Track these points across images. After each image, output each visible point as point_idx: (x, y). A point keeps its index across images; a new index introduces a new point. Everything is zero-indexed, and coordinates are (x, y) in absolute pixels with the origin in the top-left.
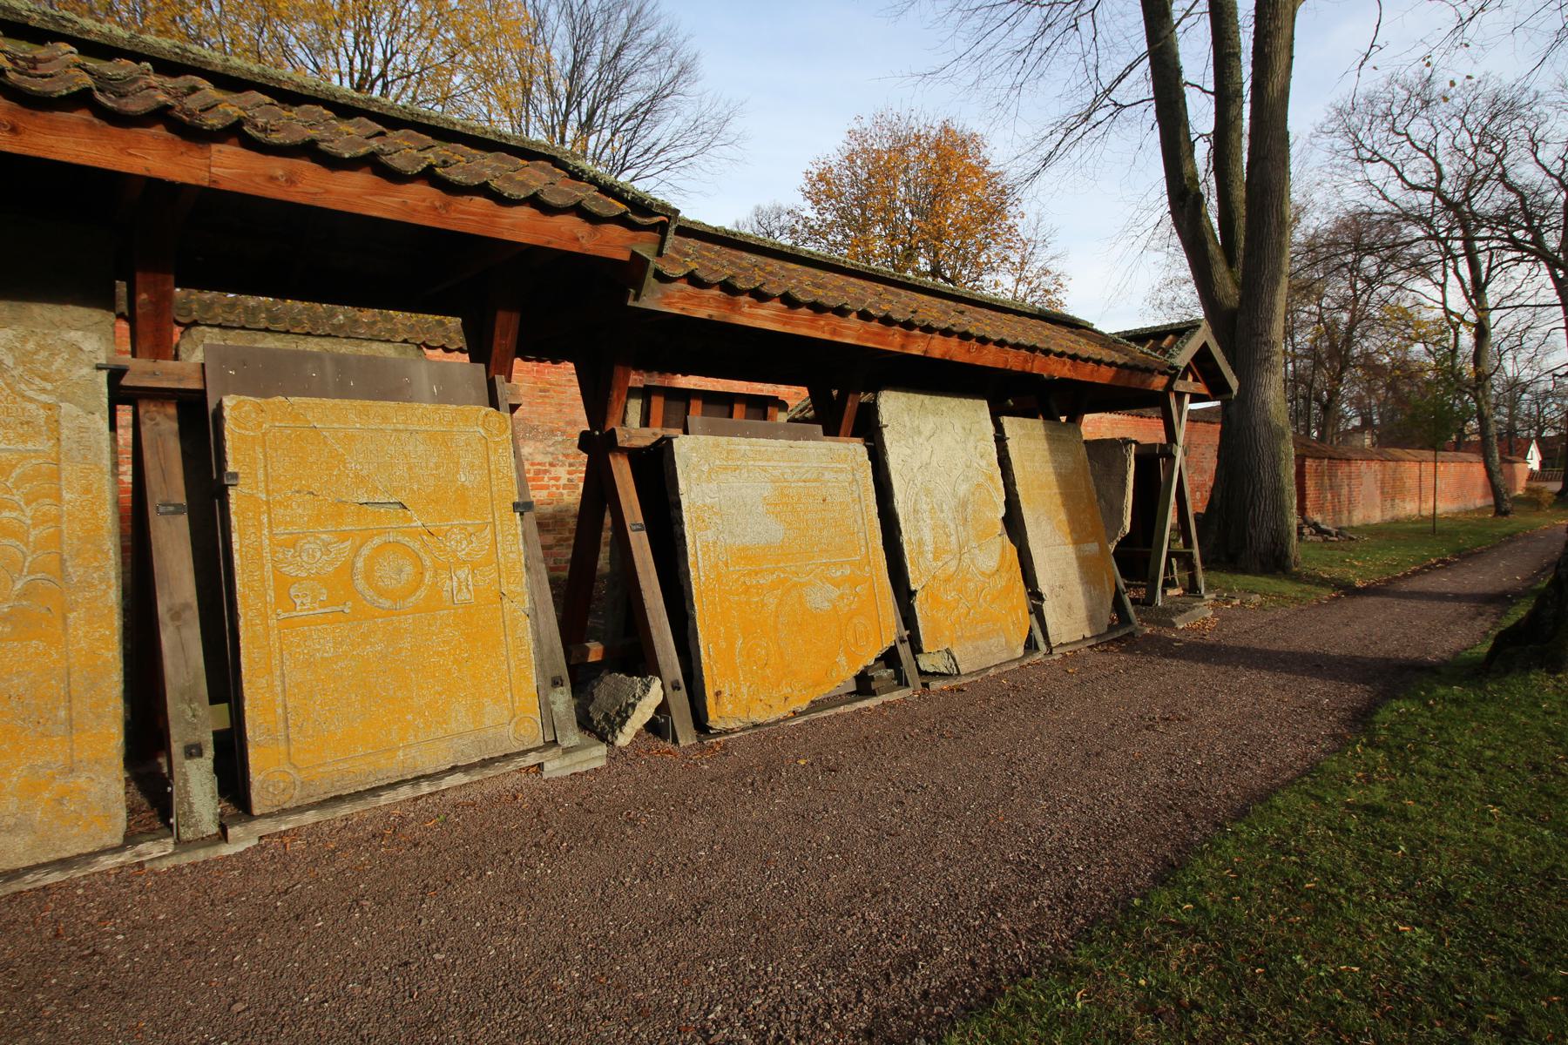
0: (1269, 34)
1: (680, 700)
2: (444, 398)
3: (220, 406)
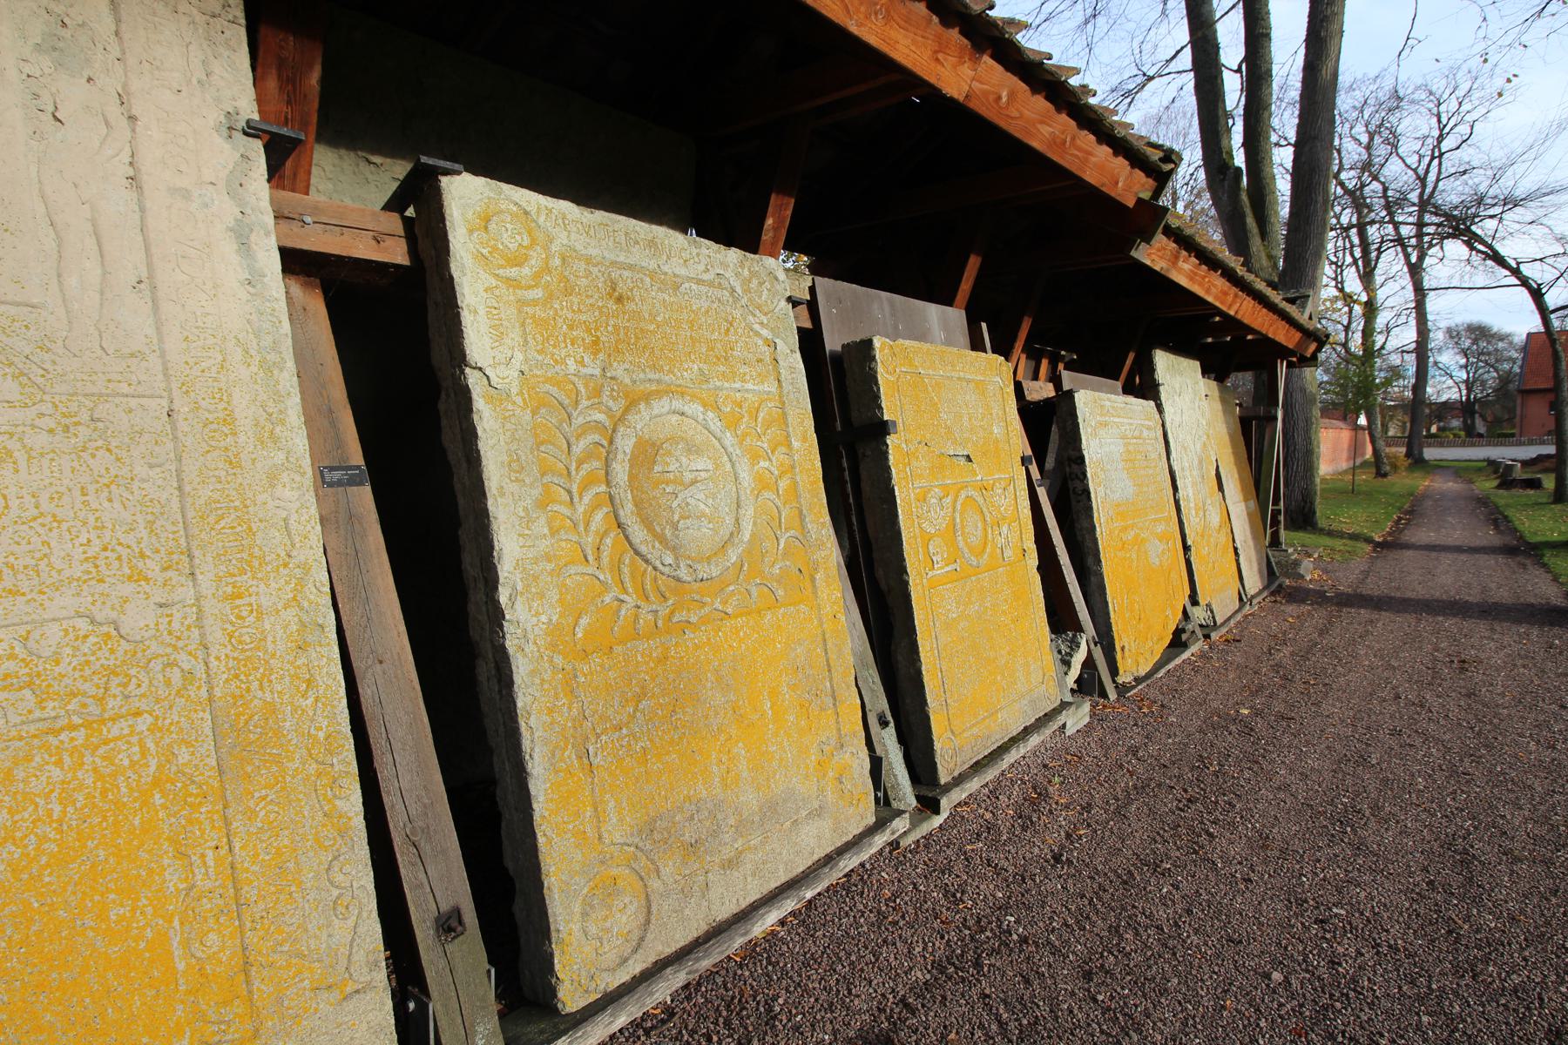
0: (1326, 19)
1: (1098, 654)
2: (949, 342)
3: (864, 350)
